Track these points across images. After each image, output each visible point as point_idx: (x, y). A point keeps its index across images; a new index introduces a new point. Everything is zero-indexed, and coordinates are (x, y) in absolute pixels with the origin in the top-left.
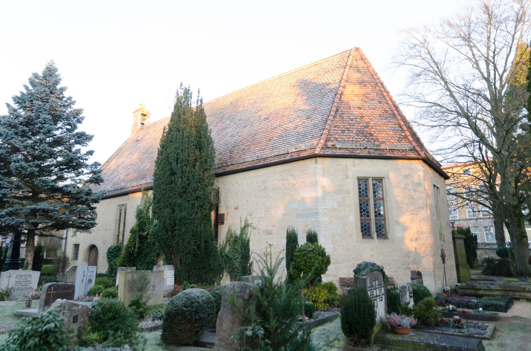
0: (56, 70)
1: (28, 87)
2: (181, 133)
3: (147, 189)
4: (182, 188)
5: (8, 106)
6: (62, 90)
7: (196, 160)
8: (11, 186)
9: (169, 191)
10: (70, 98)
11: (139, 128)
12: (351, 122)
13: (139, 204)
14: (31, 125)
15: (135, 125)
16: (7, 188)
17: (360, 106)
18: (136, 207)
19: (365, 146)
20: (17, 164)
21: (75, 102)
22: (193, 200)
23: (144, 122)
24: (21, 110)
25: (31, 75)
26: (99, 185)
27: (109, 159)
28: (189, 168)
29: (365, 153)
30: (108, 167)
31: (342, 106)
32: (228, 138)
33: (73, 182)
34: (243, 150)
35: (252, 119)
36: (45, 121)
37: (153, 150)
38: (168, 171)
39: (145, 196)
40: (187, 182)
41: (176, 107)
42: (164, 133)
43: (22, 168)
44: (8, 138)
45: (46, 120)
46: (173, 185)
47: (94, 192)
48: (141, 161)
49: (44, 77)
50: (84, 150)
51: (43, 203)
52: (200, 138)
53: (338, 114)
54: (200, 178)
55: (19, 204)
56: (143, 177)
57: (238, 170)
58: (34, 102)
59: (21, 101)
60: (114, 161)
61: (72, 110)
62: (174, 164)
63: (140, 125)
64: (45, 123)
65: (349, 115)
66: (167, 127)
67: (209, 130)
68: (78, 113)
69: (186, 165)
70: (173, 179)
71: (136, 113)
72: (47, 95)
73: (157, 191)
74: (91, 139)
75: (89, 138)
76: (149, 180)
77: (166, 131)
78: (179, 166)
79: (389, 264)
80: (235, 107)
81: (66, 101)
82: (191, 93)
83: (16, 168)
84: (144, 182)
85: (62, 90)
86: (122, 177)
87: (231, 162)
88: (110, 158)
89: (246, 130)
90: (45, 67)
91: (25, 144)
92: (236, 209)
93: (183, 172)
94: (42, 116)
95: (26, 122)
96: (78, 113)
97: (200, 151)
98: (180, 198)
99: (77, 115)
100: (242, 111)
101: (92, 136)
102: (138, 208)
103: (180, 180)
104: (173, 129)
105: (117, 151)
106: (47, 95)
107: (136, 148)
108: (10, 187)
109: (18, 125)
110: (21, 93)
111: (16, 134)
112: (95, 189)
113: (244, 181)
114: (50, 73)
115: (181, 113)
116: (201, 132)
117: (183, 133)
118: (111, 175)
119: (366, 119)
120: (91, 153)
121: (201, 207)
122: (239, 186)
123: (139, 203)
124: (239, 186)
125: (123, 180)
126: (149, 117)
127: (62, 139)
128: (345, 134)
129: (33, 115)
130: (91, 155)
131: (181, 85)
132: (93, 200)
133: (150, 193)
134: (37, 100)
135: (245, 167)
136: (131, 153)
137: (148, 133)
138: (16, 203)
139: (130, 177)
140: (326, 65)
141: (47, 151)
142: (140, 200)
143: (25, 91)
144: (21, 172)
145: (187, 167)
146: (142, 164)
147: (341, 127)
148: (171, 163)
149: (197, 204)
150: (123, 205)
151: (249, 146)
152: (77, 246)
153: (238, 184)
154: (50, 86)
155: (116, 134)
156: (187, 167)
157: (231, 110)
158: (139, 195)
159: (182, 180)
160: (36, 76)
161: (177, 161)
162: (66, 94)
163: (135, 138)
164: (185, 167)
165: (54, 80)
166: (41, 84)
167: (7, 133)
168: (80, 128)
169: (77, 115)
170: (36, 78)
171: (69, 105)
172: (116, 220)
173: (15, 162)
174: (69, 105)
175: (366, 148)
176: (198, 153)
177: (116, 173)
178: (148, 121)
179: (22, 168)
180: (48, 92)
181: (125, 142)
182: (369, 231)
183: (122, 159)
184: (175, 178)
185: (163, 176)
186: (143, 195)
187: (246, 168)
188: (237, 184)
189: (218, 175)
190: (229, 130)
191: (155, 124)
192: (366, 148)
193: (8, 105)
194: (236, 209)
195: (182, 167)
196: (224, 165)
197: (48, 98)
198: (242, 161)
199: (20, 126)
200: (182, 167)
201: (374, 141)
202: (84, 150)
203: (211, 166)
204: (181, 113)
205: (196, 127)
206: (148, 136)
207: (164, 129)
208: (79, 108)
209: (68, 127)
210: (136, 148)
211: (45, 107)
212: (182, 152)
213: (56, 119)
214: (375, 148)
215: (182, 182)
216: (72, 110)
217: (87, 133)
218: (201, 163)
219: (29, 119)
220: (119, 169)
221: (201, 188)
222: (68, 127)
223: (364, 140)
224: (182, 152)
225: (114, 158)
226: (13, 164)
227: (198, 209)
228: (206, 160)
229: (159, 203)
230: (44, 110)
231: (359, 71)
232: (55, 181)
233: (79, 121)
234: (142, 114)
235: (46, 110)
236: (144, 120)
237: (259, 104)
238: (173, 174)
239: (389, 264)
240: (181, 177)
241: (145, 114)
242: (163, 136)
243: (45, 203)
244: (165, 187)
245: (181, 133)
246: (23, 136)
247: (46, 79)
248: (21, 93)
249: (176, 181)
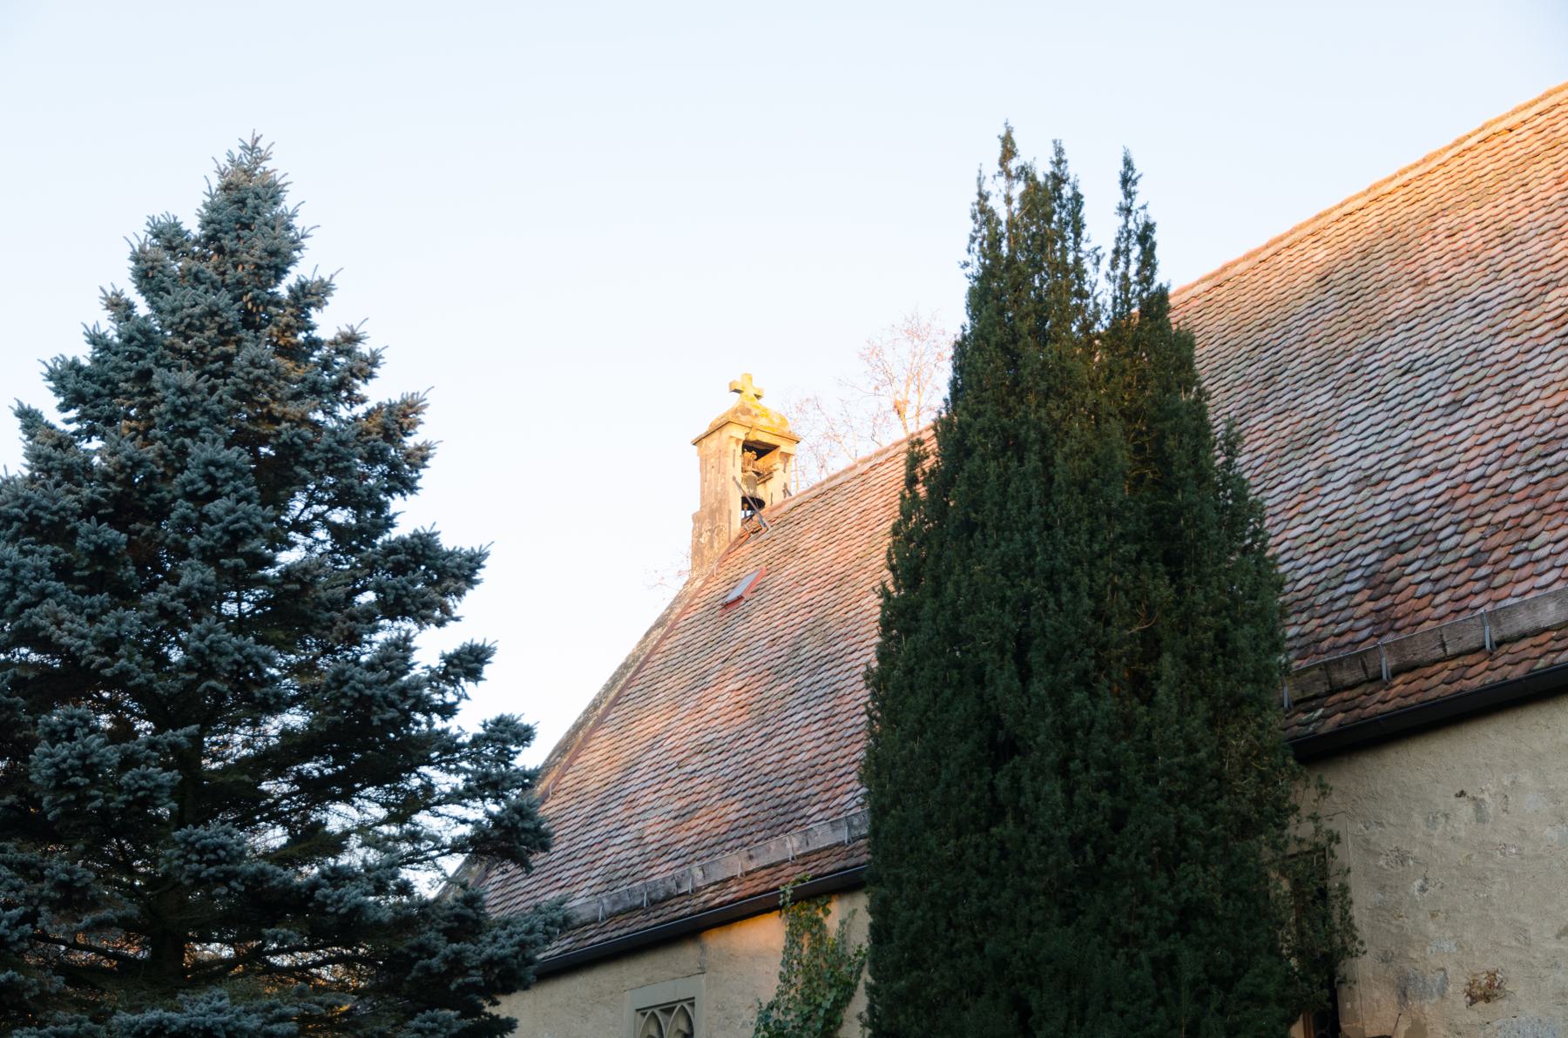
0: (272, 193)
1: (130, 306)
2: (1033, 461)
3: (818, 892)
4: (1076, 844)
5: (26, 428)
6: (311, 295)
7: (1151, 646)
9: (983, 872)
10: (346, 344)
11: (737, 526)
13: (768, 996)
14: (140, 515)
15: (710, 516)
18: (751, 1016)
20: (62, 750)
22: (1164, 933)
23: (761, 492)
25: (139, 234)
26: (528, 868)
28: (1108, 704)
30: (568, 781)
32: (1339, 496)
33: (373, 856)
34: (1476, 560)
35: (1505, 348)
36: (210, 479)
37: (830, 643)
38: (963, 735)
39: (806, 940)
40: (1104, 799)
41: (982, 298)
42: (911, 481)
44: (22, 596)
45: (220, 475)
46: (1007, 829)
47: (494, 913)
48: (764, 722)
49: (211, 238)
50: (430, 647)
51: (204, 996)
52: (1166, 486)
54: (1195, 769)
55: (79, 1004)
56: (785, 817)
57: (1461, 697)
58: (159, 376)
59: (90, 388)
61: (360, 410)
62: (1003, 679)
63: (739, 514)
64: (212, 496)
66: (932, 445)
67: (1219, 430)
68: (398, 419)
69: (1085, 681)
70: (1003, 783)
71: (712, 443)
72: (225, 334)
73: (898, 883)
75: (459, 572)
76: (835, 821)
77: (927, 464)
78: (1037, 687)
80: (1354, 295)
81: (326, 364)
82: (1077, 198)
83: (60, 775)
84: (792, 845)
85: (311, 295)
86: (654, 828)
87: (1398, 647)
88: (578, 727)
89: (1466, 427)
90: (216, 182)
91: (107, 625)
92: (1485, 993)
93: (1067, 734)
94: (201, 451)
95: (117, 500)
96: (398, 419)
97: (1175, 577)
98: (1067, 921)
100: (1409, 316)
102: (764, 1018)
103: (1053, 789)
104: (973, 438)
105: (614, 680)
106: (225, 334)
107: (724, 650)
108: (28, 899)
109: (73, 522)
111: (63, 571)
112: (509, 894)
113: (1526, 778)
114: (247, 216)
115: (1024, 327)
116: (1171, 442)
117: (1047, 461)
118: (589, 822)
121: (1227, 984)
122: (1481, 818)
123: (769, 989)
124: (1481, 818)
125: (664, 850)
126: (786, 456)
127: (306, 586)
129: (151, 452)
130: (474, 675)
131: (1008, 151)
133: (848, 921)
134: (169, 367)
135: (1519, 672)
136: (700, 682)
137: (791, 551)
138: (61, 1000)
139: (700, 823)
142: (775, 966)
143: (109, 328)
145: (1094, 695)
146: (768, 737)
148: (980, 679)
149: (1190, 965)
150: (668, 1009)
151: (1518, 522)
153: (1478, 804)
154: (240, 283)
155: (623, 492)
156: (1094, 695)
157: (1351, 292)
158: (766, 936)
159: (1069, 792)
160: (169, 237)
161: (1020, 657)
162: (326, 324)
163: (717, 588)
164: (1079, 697)
165: (260, 244)
166: (197, 278)
167: (16, 569)
168: (408, 516)
169: (389, 436)
170: (170, 247)
171: (337, 387)
173: (53, 736)
174: (337, 387)
176: (1163, 591)
177: (616, 809)
178: (793, 479)
180: (233, 315)
181: (659, 624)
183: (651, 724)
184: (1016, 779)
185: (934, 773)
186: (793, 937)
187: (1533, 676)
188: (1466, 810)
189: (1326, 751)
190: (1338, 447)
191: (825, 494)
193: (30, 419)
194: (1485, 993)
195: (1059, 697)
196: (1348, 677)
197: (231, 349)
198: (1489, 634)
199: (84, 527)
200: (1059, 697)
202: (430, 647)
203: (1264, 677)
204: (1024, 327)
205: (1130, 416)
206: (793, 568)
207: (914, 460)
208: (397, 399)
209: (340, 516)
210: (724, 650)
211: (212, 403)
212: (1055, 590)
213: (276, 481)
215: (1070, 805)
216: (360, 410)
217: (447, 543)
218: (1192, 660)
220: (635, 782)
221: (1214, 840)
222: (340, 516)
224: (1055, 590)
225: (599, 723)
227: (1201, 997)
228: (1222, 638)
229: (914, 964)
230: (233, 408)
232: (281, 857)
233: (405, 485)
234: (748, 446)
235: (216, 419)
236: (763, 477)
237: (1535, 246)
238: (1002, 749)
240: (1063, 769)
241: (766, 438)
242: (909, 505)
243: (218, 991)
244: (949, 852)
245: (1033, 461)
246: (94, 585)
247: (220, 250)
249: (1027, 800)
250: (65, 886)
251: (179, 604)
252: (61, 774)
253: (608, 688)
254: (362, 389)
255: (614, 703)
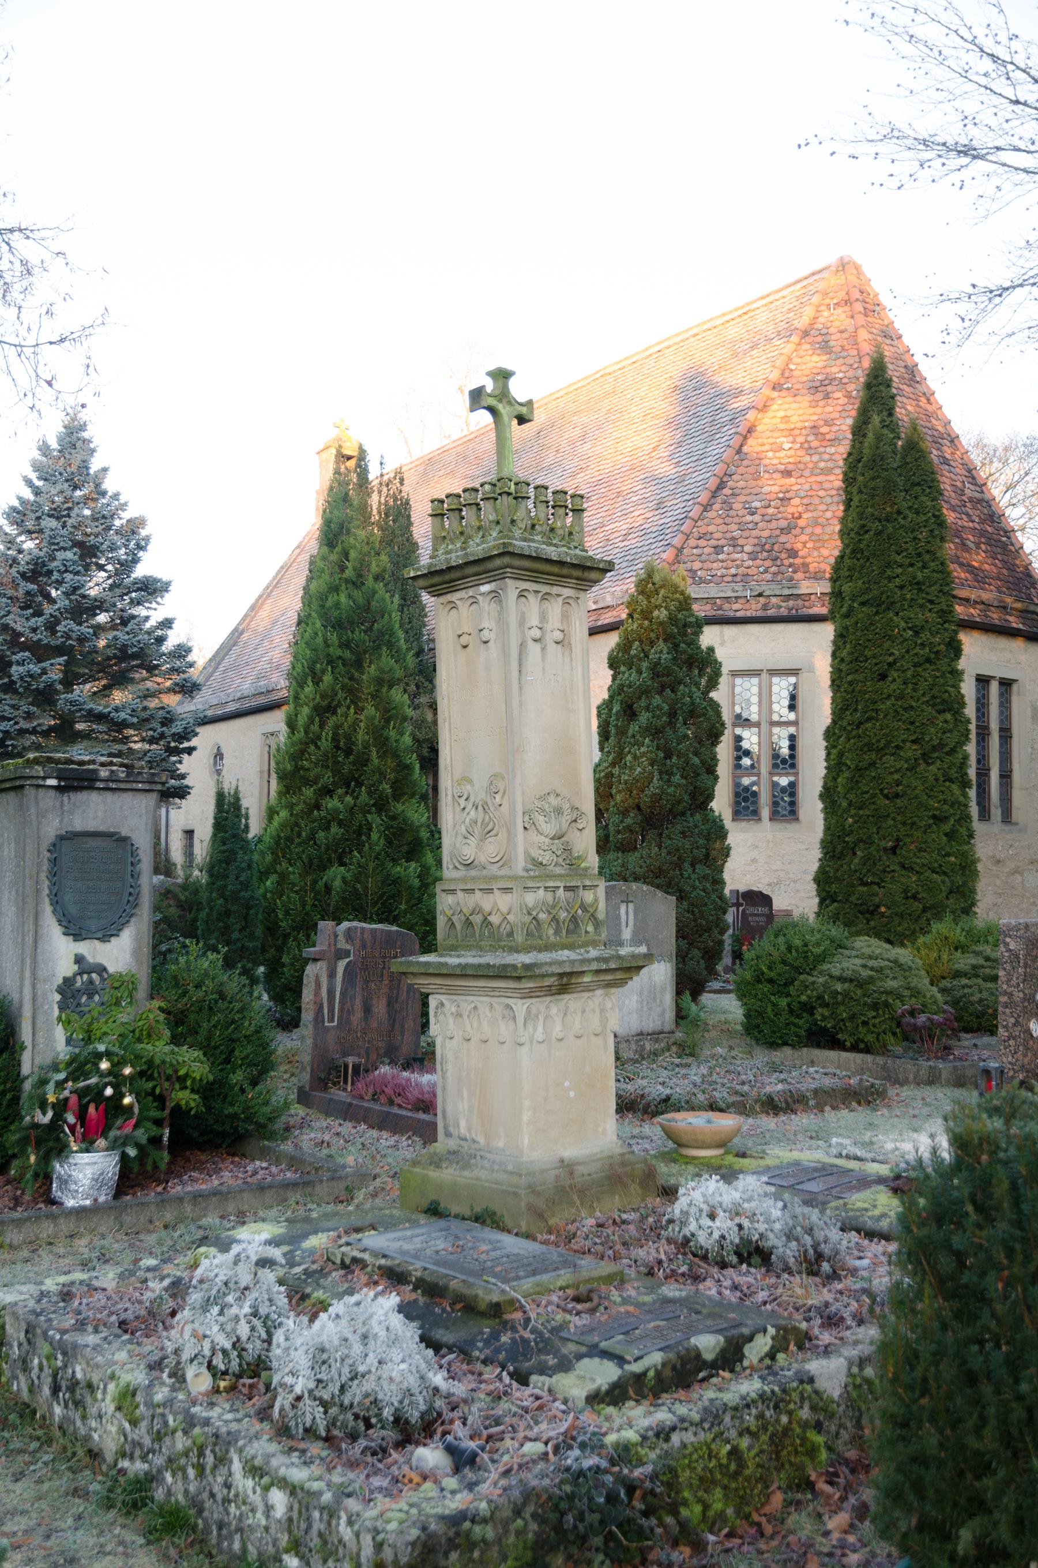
8: (16, 713)
12: (749, 518)
14: (41, 574)
16: (10, 719)
17: (790, 467)
19: (759, 590)
21: (126, 504)
24: (23, 538)
27: (257, 601)
29: (754, 609)
31: (741, 470)
43: (31, 676)
53: (719, 500)
60: (267, 607)
65: (749, 498)
71: (324, 455)
74: (167, 591)
79: (795, 882)
88: (260, 597)
95: (33, 571)
99: (133, 533)
101: (168, 584)
110: (19, 498)
114: (74, 440)
119: (795, 506)
120: (167, 624)
128: (721, 557)
132: (174, 735)
140: (733, 332)
141: (74, 635)
144: (30, 685)
147: (715, 536)
152: (189, 833)
155: (221, 579)
172: (261, 772)
175: (760, 595)
179: (31, 676)
181: (298, 547)
182: (755, 803)
192: (760, 595)
201: (795, 572)
214: (787, 592)
219: (36, 564)
223: (766, 571)
225: (269, 595)
226: (14, 668)
230: (75, 522)
231: (825, 348)
239: (795, 882)
248: (19, 498)
250: (28, 713)
251: (57, 613)
252: (22, 678)
253: (274, 578)
254: (122, 514)
255: (275, 587)
